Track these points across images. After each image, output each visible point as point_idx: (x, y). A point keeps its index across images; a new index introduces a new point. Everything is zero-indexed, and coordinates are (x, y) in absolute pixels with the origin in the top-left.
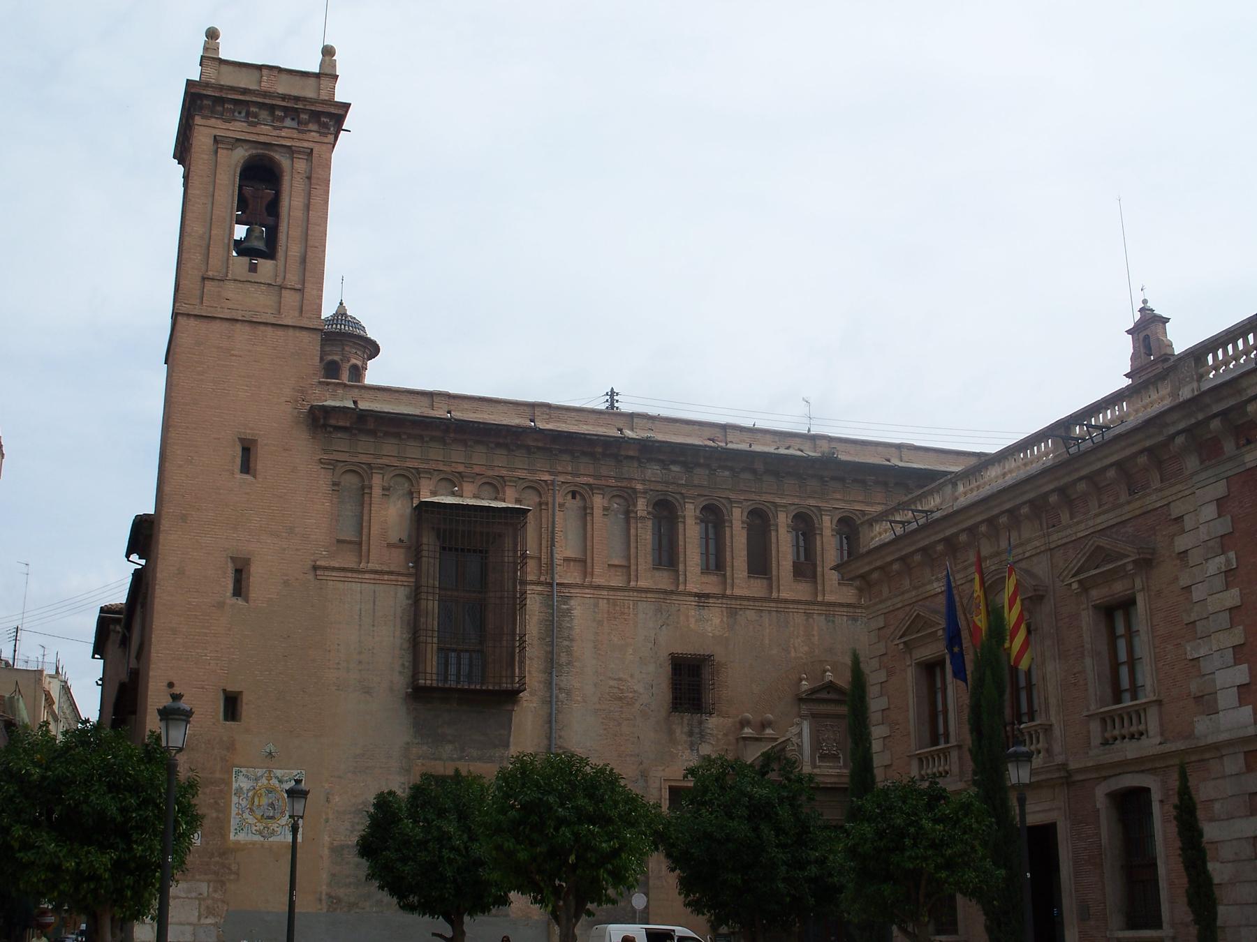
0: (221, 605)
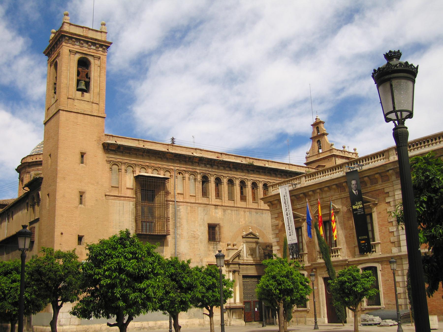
0: (77, 207)
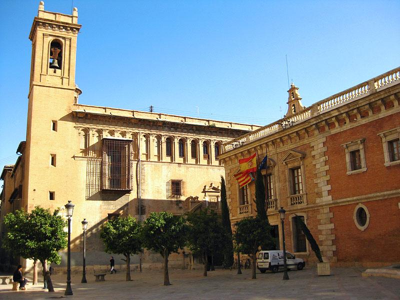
0: (48, 168)
